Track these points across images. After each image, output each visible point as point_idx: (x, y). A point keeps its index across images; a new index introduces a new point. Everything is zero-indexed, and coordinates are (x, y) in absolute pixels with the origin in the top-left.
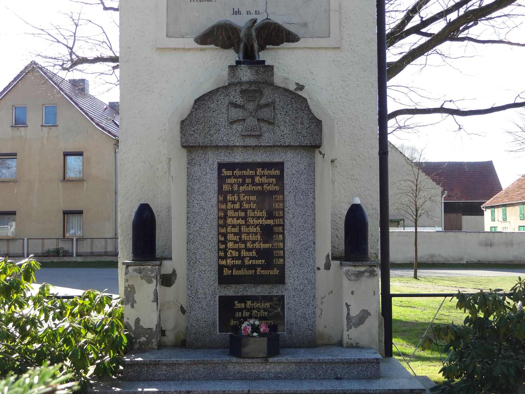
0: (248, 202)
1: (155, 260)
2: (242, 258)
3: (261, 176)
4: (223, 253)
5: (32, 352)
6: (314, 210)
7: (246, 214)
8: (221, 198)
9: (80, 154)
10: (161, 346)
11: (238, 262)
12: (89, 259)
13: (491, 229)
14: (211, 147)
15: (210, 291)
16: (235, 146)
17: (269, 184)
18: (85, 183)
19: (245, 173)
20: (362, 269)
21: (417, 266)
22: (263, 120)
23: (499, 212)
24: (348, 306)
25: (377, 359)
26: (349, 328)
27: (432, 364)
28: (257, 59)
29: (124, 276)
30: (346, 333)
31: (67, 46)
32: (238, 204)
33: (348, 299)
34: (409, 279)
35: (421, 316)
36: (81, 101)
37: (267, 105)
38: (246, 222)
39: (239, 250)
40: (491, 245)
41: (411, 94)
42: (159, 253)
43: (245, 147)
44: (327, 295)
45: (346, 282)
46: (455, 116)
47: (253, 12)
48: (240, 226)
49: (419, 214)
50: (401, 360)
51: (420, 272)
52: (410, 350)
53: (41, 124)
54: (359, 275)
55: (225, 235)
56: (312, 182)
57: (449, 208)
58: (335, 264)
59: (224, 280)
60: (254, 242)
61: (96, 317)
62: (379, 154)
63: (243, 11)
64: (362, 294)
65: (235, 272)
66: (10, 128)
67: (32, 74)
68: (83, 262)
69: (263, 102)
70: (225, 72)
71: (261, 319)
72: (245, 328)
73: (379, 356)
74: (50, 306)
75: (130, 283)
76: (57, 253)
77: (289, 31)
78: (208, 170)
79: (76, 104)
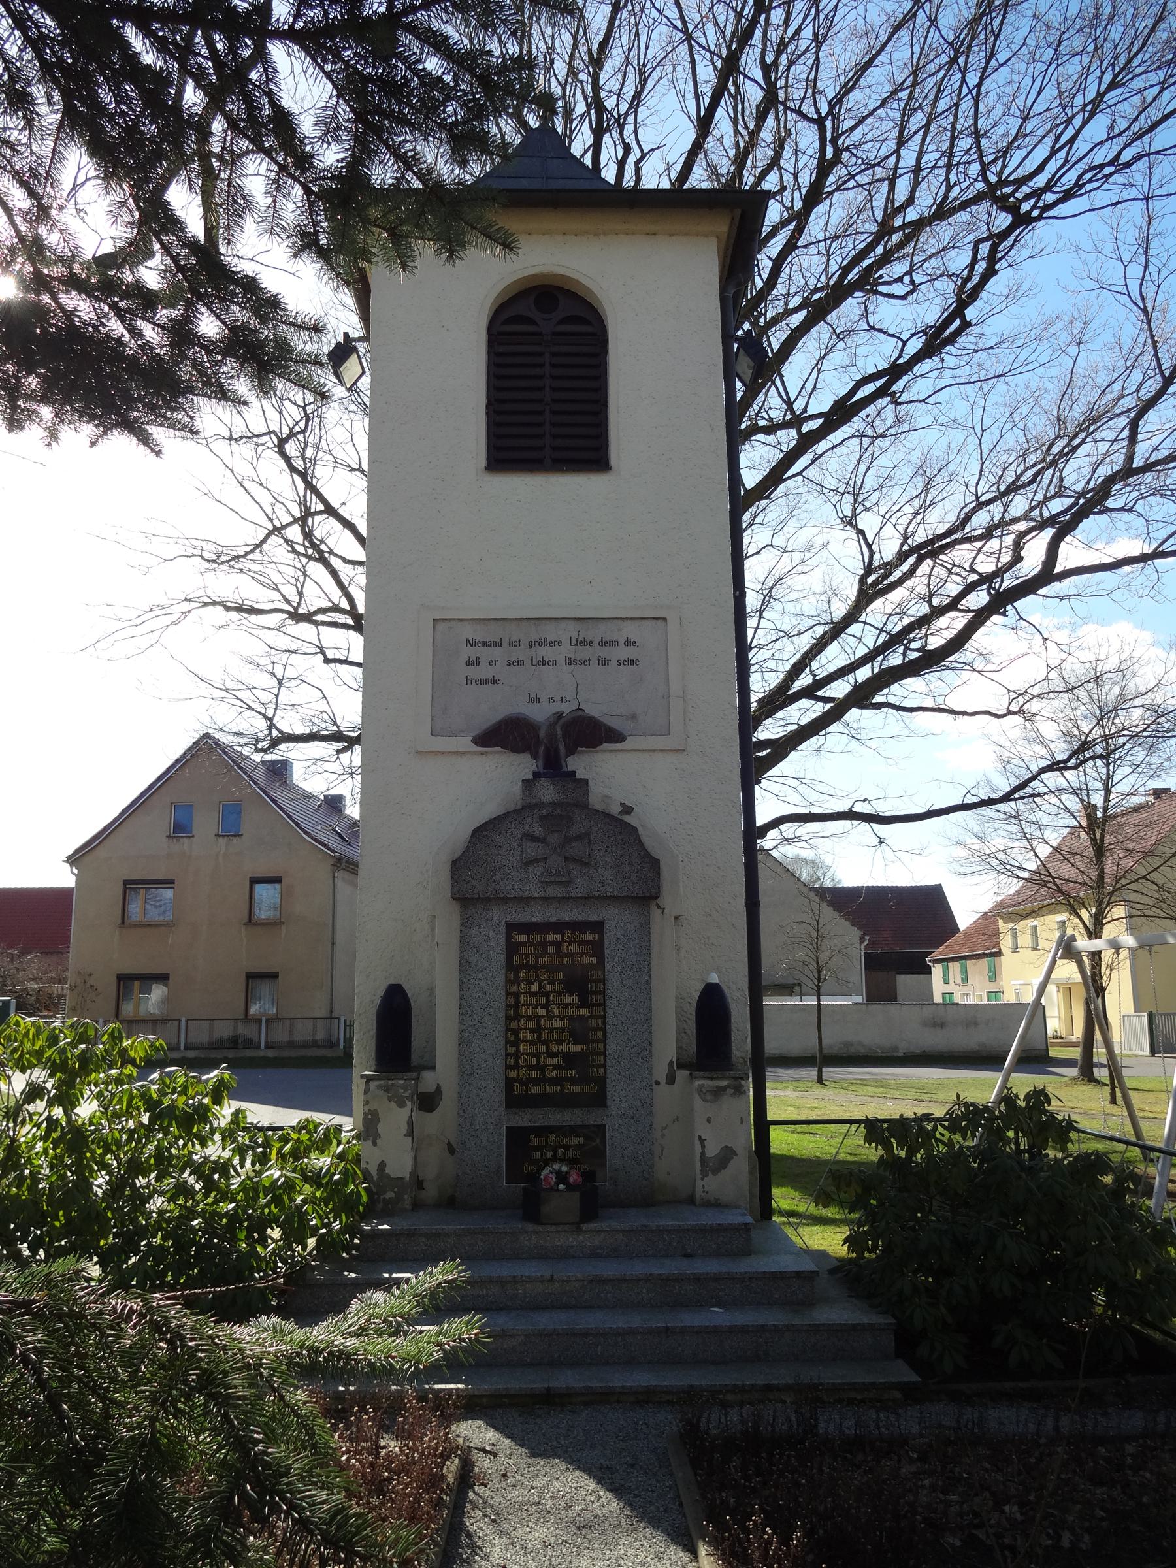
0: (551, 982)
1: (410, 1071)
2: (541, 1068)
3: (570, 943)
4: (512, 1060)
5: (221, 1216)
6: (649, 993)
7: (548, 1000)
8: (511, 976)
9: (277, 880)
10: (417, 1206)
11: (535, 1074)
12: (287, 1053)
13: (944, 998)
14: (496, 899)
15: (493, 1118)
16: (531, 898)
17: (582, 954)
18: (283, 928)
19: (547, 937)
20: (724, 1083)
21: (822, 1060)
22: (574, 860)
23: (955, 969)
24: (702, 1141)
25: (746, 1225)
26: (704, 1175)
27: (839, 1230)
28: (564, 769)
29: (362, 1097)
30: (699, 1184)
31: (264, 715)
32: (536, 985)
33: (702, 1129)
34: (810, 1084)
35: (826, 1149)
36: (280, 795)
37: (579, 837)
38: (548, 1012)
39: (537, 1055)
40: (942, 1025)
41: (802, 788)
42: (415, 1059)
43: (545, 899)
44: (673, 1124)
45: (698, 1102)
46: (873, 825)
47: (557, 698)
48: (539, 1017)
49: (822, 977)
50: (784, 1223)
51: (828, 1072)
52: (803, 1205)
53: (215, 832)
54: (718, 1093)
55: (516, 1032)
56: (646, 950)
57: (873, 963)
58: (682, 1075)
59: (513, 1101)
60: (559, 1043)
61: (323, 1161)
62: (747, 905)
63: (544, 698)
64: (720, 1125)
65: (531, 1090)
66: (165, 840)
67: (205, 753)
68: (275, 1058)
69: (572, 832)
70: (518, 788)
71: (572, 1162)
72: (546, 1177)
73: (749, 1219)
74: (247, 1142)
75: (372, 1106)
76: (234, 1043)
77: (609, 727)
78: (491, 933)
79: (273, 801)
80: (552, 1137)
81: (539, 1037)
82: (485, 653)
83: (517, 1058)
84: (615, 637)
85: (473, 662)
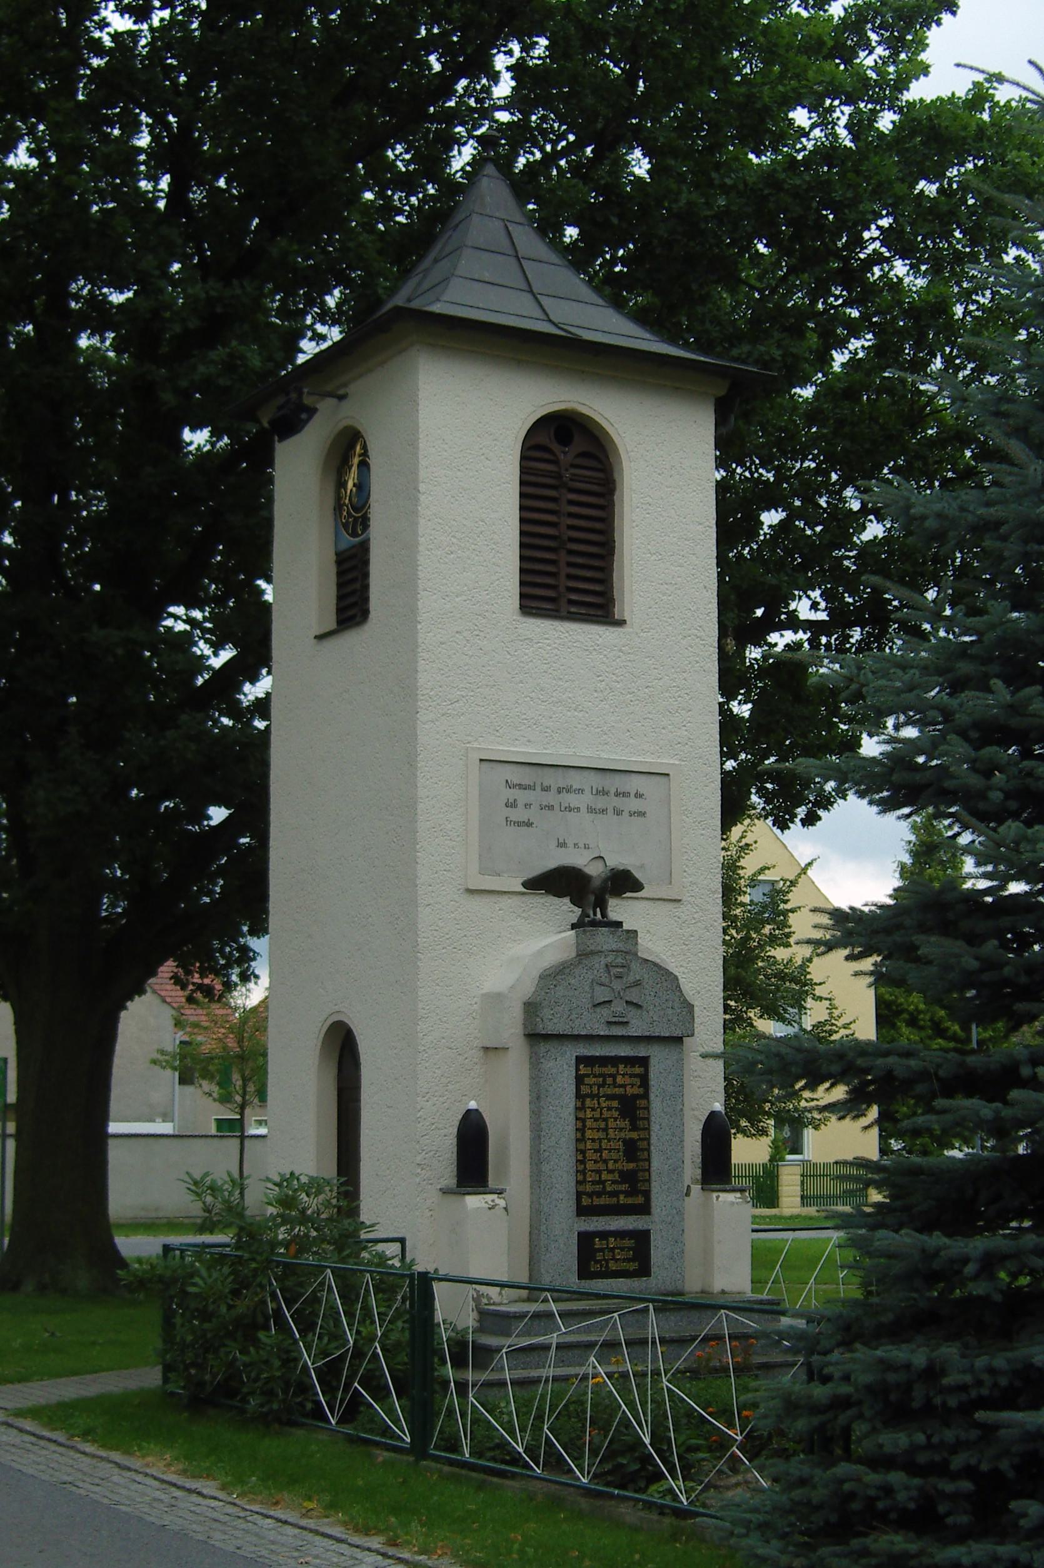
3: (623, 1075)
7: (607, 1125)
8: (579, 1104)
11: (598, 1188)
48: (600, 1140)
59: (582, 1211)
60: (616, 1161)
82: (522, 796)
83: (585, 1174)
84: (627, 789)
85: (512, 805)
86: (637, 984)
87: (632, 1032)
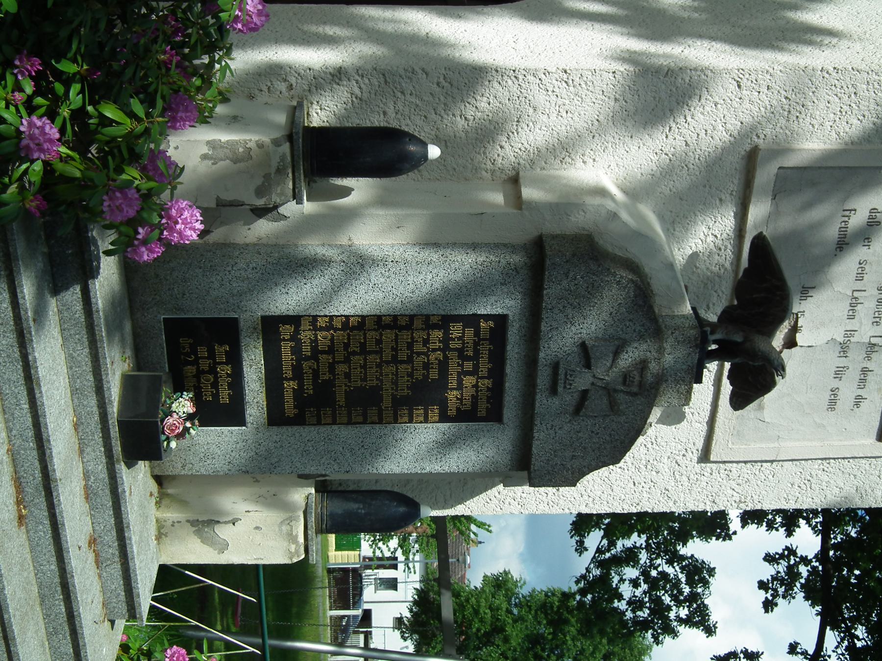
38: (388, 363)
48: (380, 352)
60: (348, 376)
80: (228, 369)
81: (354, 353)
86: (613, 406)
87: (543, 402)
